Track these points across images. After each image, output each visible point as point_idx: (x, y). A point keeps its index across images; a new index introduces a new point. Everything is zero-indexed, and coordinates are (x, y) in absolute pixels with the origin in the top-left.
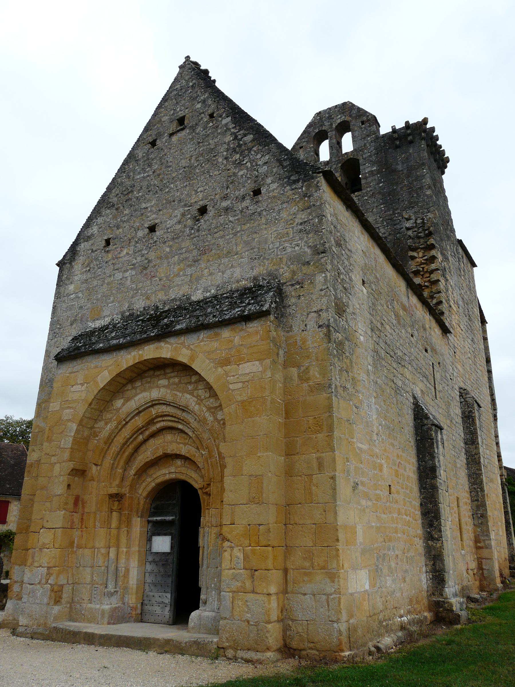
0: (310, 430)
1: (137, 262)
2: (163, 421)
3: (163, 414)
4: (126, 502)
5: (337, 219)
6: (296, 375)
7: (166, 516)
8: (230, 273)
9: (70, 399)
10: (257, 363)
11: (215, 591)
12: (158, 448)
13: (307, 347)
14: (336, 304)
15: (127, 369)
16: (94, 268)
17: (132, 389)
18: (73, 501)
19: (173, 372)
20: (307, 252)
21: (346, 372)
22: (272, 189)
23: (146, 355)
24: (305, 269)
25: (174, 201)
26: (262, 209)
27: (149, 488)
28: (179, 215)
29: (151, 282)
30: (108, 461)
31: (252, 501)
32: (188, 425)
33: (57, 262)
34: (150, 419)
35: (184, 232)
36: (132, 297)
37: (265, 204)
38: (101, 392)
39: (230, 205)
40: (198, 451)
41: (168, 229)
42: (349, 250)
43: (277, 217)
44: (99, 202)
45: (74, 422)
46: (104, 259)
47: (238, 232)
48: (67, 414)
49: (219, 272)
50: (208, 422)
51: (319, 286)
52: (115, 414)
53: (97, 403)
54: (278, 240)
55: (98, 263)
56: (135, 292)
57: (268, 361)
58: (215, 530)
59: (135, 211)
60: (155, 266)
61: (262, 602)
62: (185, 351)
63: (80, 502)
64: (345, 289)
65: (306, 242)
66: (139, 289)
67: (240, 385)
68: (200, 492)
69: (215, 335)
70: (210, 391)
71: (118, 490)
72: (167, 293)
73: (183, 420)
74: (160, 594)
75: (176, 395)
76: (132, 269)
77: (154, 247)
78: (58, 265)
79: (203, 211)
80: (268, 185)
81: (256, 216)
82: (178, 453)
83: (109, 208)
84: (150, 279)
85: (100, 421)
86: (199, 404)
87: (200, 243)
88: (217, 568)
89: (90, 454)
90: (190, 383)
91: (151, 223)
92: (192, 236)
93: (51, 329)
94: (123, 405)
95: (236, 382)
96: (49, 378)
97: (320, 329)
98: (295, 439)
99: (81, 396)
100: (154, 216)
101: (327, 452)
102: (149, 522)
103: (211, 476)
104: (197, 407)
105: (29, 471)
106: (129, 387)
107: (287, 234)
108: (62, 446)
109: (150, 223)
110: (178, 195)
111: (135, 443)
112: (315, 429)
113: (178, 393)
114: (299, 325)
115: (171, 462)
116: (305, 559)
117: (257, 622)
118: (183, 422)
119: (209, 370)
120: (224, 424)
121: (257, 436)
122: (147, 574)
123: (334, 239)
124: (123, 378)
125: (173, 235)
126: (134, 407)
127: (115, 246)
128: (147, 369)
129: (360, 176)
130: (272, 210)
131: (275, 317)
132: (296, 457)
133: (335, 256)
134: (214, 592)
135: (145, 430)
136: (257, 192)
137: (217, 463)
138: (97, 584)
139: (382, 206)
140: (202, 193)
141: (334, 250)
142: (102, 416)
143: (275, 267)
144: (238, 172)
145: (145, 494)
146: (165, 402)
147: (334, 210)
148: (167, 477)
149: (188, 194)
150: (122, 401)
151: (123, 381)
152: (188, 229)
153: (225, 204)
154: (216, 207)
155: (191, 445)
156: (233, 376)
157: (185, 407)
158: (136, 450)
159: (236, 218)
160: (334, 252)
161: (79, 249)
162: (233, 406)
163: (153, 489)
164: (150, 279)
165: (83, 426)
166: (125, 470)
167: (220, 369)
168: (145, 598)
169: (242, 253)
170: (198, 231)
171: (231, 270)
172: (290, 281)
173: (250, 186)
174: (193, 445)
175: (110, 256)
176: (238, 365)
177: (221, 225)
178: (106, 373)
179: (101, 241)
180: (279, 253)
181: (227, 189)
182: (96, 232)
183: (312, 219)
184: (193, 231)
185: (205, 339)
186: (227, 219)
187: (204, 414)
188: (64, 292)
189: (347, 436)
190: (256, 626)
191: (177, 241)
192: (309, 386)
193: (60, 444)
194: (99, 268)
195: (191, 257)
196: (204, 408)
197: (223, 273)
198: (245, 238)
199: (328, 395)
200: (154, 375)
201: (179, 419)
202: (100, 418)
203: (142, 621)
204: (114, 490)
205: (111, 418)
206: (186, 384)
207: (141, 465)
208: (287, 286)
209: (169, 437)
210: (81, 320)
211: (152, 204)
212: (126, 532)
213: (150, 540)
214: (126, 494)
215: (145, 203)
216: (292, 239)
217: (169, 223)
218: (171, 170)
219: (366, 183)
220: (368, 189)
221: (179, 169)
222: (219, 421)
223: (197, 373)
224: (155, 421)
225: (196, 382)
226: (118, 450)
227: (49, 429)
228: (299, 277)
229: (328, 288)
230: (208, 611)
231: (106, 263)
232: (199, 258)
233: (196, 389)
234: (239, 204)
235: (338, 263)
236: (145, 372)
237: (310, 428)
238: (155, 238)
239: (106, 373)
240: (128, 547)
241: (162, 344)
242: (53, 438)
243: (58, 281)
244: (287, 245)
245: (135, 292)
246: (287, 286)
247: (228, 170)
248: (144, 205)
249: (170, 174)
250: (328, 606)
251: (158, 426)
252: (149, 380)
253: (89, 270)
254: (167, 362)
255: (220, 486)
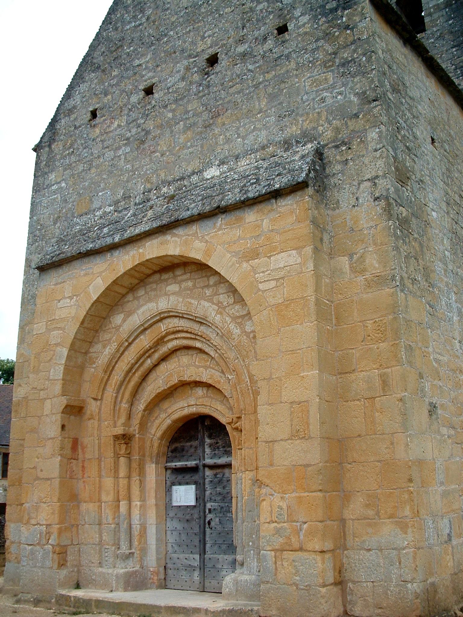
0: (369, 338)
1: (132, 136)
2: (176, 338)
3: (175, 329)
4: (135, 444)
5: (392, 56)
6: (347, 266)
7: (187, 461)
8: (253, 138)
9: (57, 318)
10: (294, 252)
11: (254, 551)
12: (171, 375)
13: (360, 227)
14: (397, 169)
15: (125, 273)
16: (79, 149)
17: (133, 300)
18: (70, 445)
19: (185, 273)
20: (354, 101)
21: (415, 259)
22: (302, 23)
23: (148, 254)
24: (352, 124)
25: (175, 52)
26: (291, 50)
27: (164, 426)
28: (182, 69)
29: (151, 159)
30: (110, 392)
31: (294, 435)
32: (208, 342)
33: (33, 147)
34: (159, 337)
35: (189, 90)
36: (128, 181)
37: (293, 44)
38: (95, 305)
39: (248, 50)
40: (223, 376)
41: (168, 89)
42: (410, 97)
43: (311, 59)
44: (81, 65)
45: (63, 347)
46: (90, 136)
47: (260, 83)
48: (55, 336)
49: (238, 137)
50: (234, 336)
51: (372, 146)
52: (115, 334)
53: (91, 321)
54: (315, 89)
55: (83, 142)
56: (131, 174)
57: (309, 250)
58: (249, 475)
59: (127, 70)
60: (155, 137)
61: (314, 561)
62: (198, 244)
63: (79, 447)
64: (408, 148)
65: (351, 88)
66: (137, 169)
67: (273, 284)
68: (228, 428)
69: (236, 220)
70: (234, 296)
71: (124, 430)
72: (172, 172)
73: (201, 336)
74: (187, 555)
75: (190, 303)
76: (125, 145)
77: (153, 113)
78: (35, 150)
79: (213, 60)
80: (297, 19)
81: (283, 61)
82: (197, 379)
83: (93, 72)
84: (150, 156)
85: (96, 343)
86: (221, 313)
87: (212, 102)
88: (255, 522)
89: (86, 386)
90: (208, 286)
91: (148, 83)
92: (201, 94)
93: (31, 232)
94: (124, 321)
95: (268, 281)
96: (31, 293)
97: (377, 203)
98: (351, 351)
99: (69, 314)
100: (150, 74)
101: (393, 366)
102: (166, 469)
103: (242, 407)
104: (218, 318)
105: (16, 411)
106: (130, 297)
107: (326, 79)
108: (51, 377)
109: (145, 83)
110: (180, 44)
111: (142, 370)
112: (376, 337)
113: (193, 301)
114: (348, 199)
115: (190, 392)
116: (367, 506)
117: (308, 585)
118: (202, 339)
119: (231, 267)
120: (254, 337)
121: (299, 349)
122: (169, 533)
123: (390, 83)
124: (122, 286)
125: (175, 95)
126: (138, 323)
127: (104, 118)
128: (151, 272)
129: (423, 14)
130: (304, 51)
131: (315, 189)
132: (353, 376)
133: (393, 106)
134: (252, 552)
135: (153, 353)
136: (282, 30)
137: (248, 389)
138: (108, 545)
139: (454, 49)
140: (211, 38)
141: (391, 97)
142: (98, 336)
143: (312, 125)
144: (256, 6)
145: (159, 434)
146: (177, 314)
147: (387, 45)
148: (186, 412)
149: (192, 42)
150: (122, 316)
151: (123, 291)
152: (194, 86)
153: (241, 49)
154: (230, 54)
155: (213, 369)
156: (263, 272)
157: (204, 319)
158: (145, 377)
159: (257, 65)
160: (390, 99)
161: (58, 127)
162: (265, 312)
163: (169, 428)
164: (150, 156)
165: (76, 351)
166: (132, 405)
167: (245, 265)
168: (168, 561)
169: (267, 111)
170: (208, 87)
171: (254, 134)
172: (334, 141)
173: (272, 22)
174: (216, 368)
175: (97, 131)
176: (269, 257)
177: (238, 76)
178: (99, 280)
179: (86, 114)
180: (316, 106)
181: (243, 29)
182: (78, 103)
183: (357, 58)
184: (201, 88)
185: (223, 227)
186: (245, 68)
187: (228, 326)
188: (44, 184)
189: (420, 344)
190: (307, 590)
191: (181, 103)
192: (366, 279)
193: (49, 375)
194: (85, 148)
195: (200, 121)
196: (227, 319)
197: (244, 139)
198: (270, 90)
199: (392, 290)
200: (160, 279)
201: (196, 335)
202: (95, 340)
203: (165, 587)
204: (119, 430)
205: (110, 339)
206: (202, 288)
207: (151, 398)
208: (329, 148)
209: (184, 359)
210: (66, 217)
211: (147, 59)
212: (138, 482)
213: (169, 491)
214: (135, 435)
215: (138, 59)
216: (333, 87)
217: (171, 81)
218: (170, 14)
219: (431, 21)
220: (435, 29)
221: (180, 11)
222: (247, 334)
223: (216, 273)
224: (165, 340)
225: (215, 285)
226: (120, 378)
227: (35, 357)
228: (344, 135)
229: (383, 147)
230: (246, 575)
231: (93, 140)
232: (211, 122)
233: (216, 294)
234: (259, 46)
235: (396, 114)
236: (149, 276)
237: (369, 336)
238: (153, 102)
239: (99, 280)
240: (143, 499)
241: (168, 237)
242: (41, 368)
243: (36, 171)
244: (325, 94)
245: (131, 174)
246: (329, 148)
247: (243, 5)
248: (137, 62)
249: (168, 18)
250: (400, 563)
251: (171, 345)
252: (154, 286)
253: (73, 152)
254: (176, 261)
255: (253, 418)
